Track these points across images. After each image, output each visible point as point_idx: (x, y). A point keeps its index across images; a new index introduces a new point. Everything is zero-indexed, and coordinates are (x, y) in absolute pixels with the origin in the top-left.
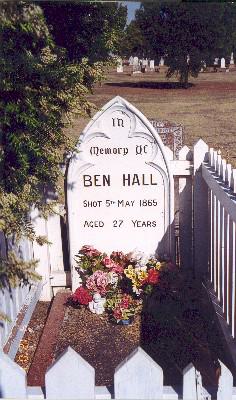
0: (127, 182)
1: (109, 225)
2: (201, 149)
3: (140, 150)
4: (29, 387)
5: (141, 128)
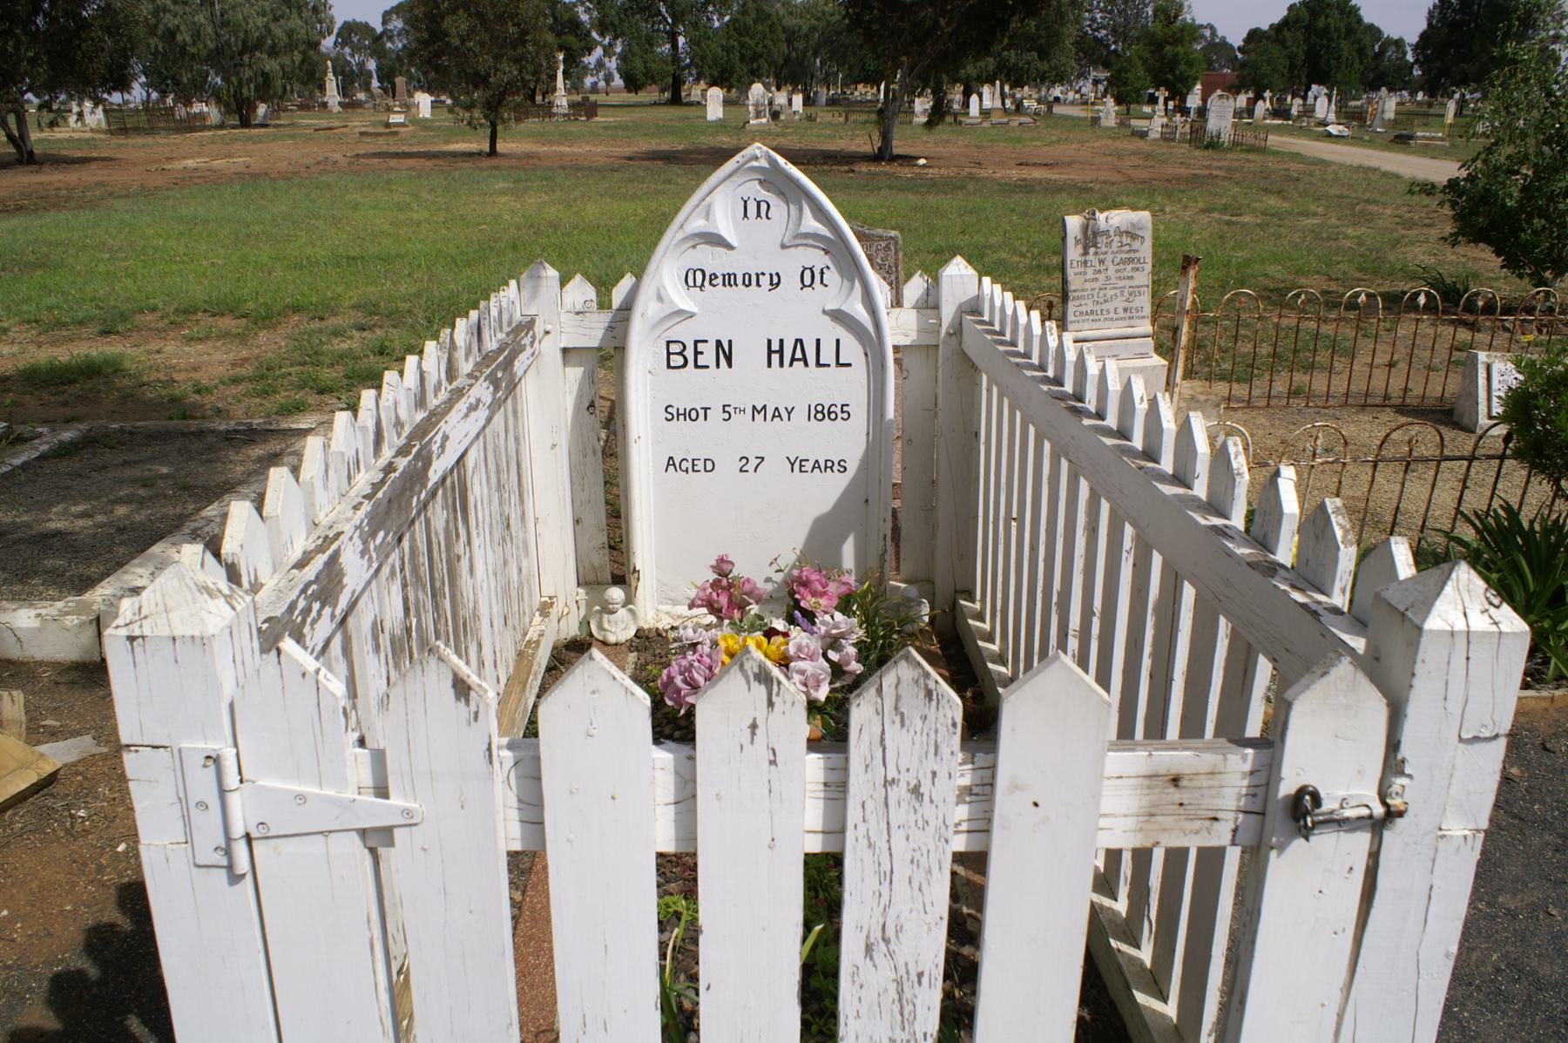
0: (775, 357)
1: (727, 465)
2: (958, 271)
3: (810, 277)
4: (802, 858)
5: (811, 224)
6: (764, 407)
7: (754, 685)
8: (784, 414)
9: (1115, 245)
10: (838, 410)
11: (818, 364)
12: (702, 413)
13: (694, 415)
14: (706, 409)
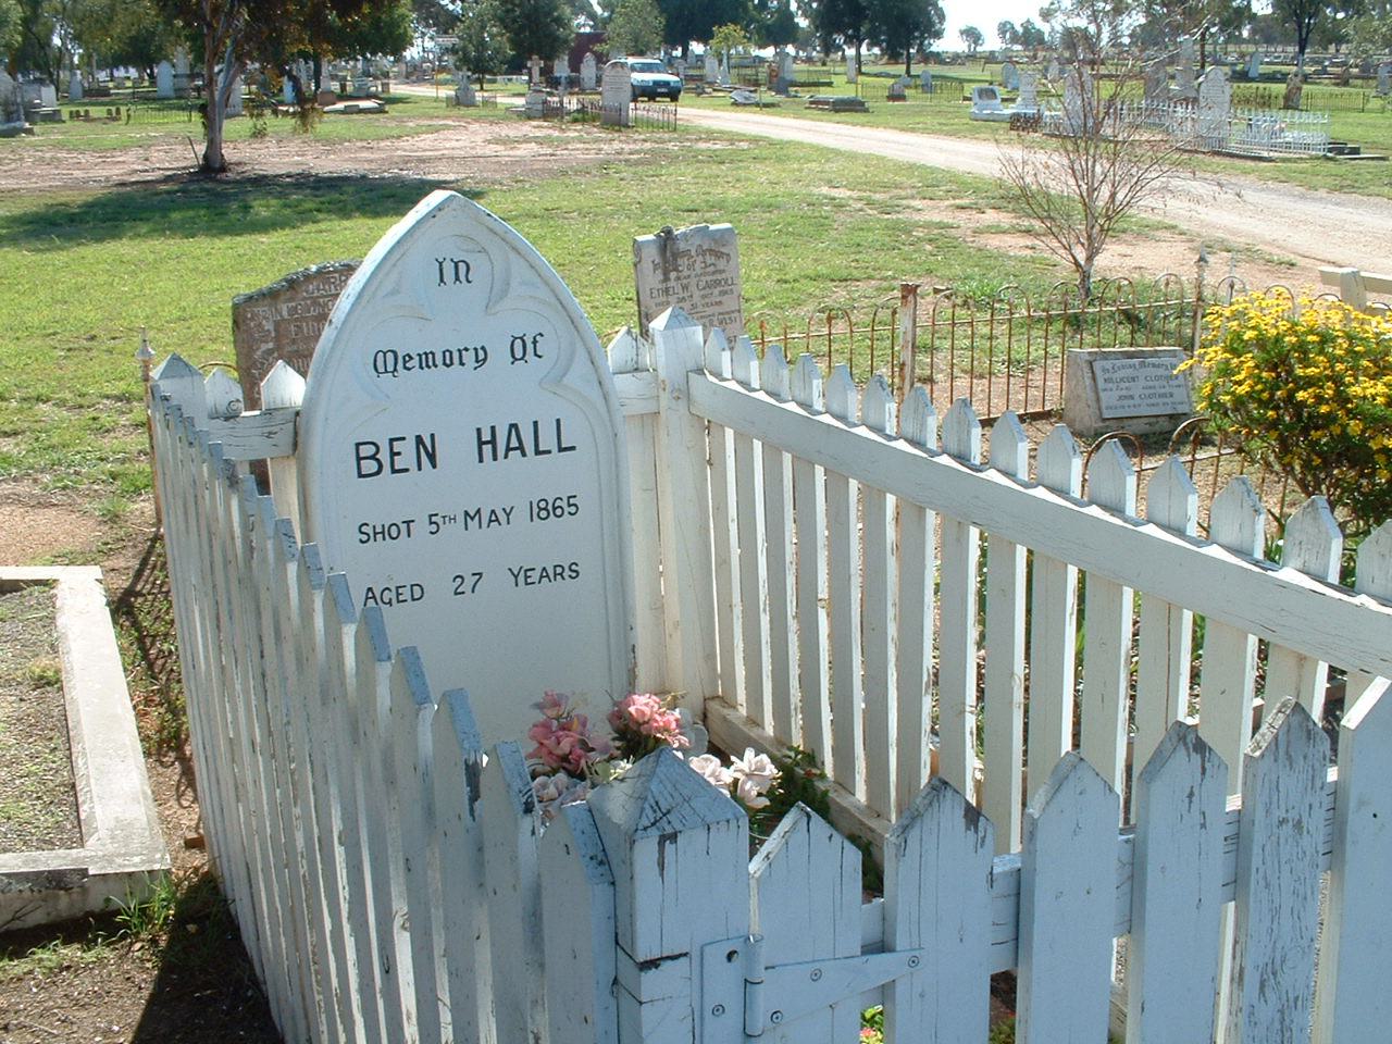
0: (487, 449)
6: (478, 511)
7: (1193, 755)
8: (502, 517)
9: (698, 266)
10: (564, 504)
11: (538, 452)
12: (403, 527)
13: (394, 532)
14: (408, 523)
